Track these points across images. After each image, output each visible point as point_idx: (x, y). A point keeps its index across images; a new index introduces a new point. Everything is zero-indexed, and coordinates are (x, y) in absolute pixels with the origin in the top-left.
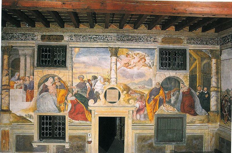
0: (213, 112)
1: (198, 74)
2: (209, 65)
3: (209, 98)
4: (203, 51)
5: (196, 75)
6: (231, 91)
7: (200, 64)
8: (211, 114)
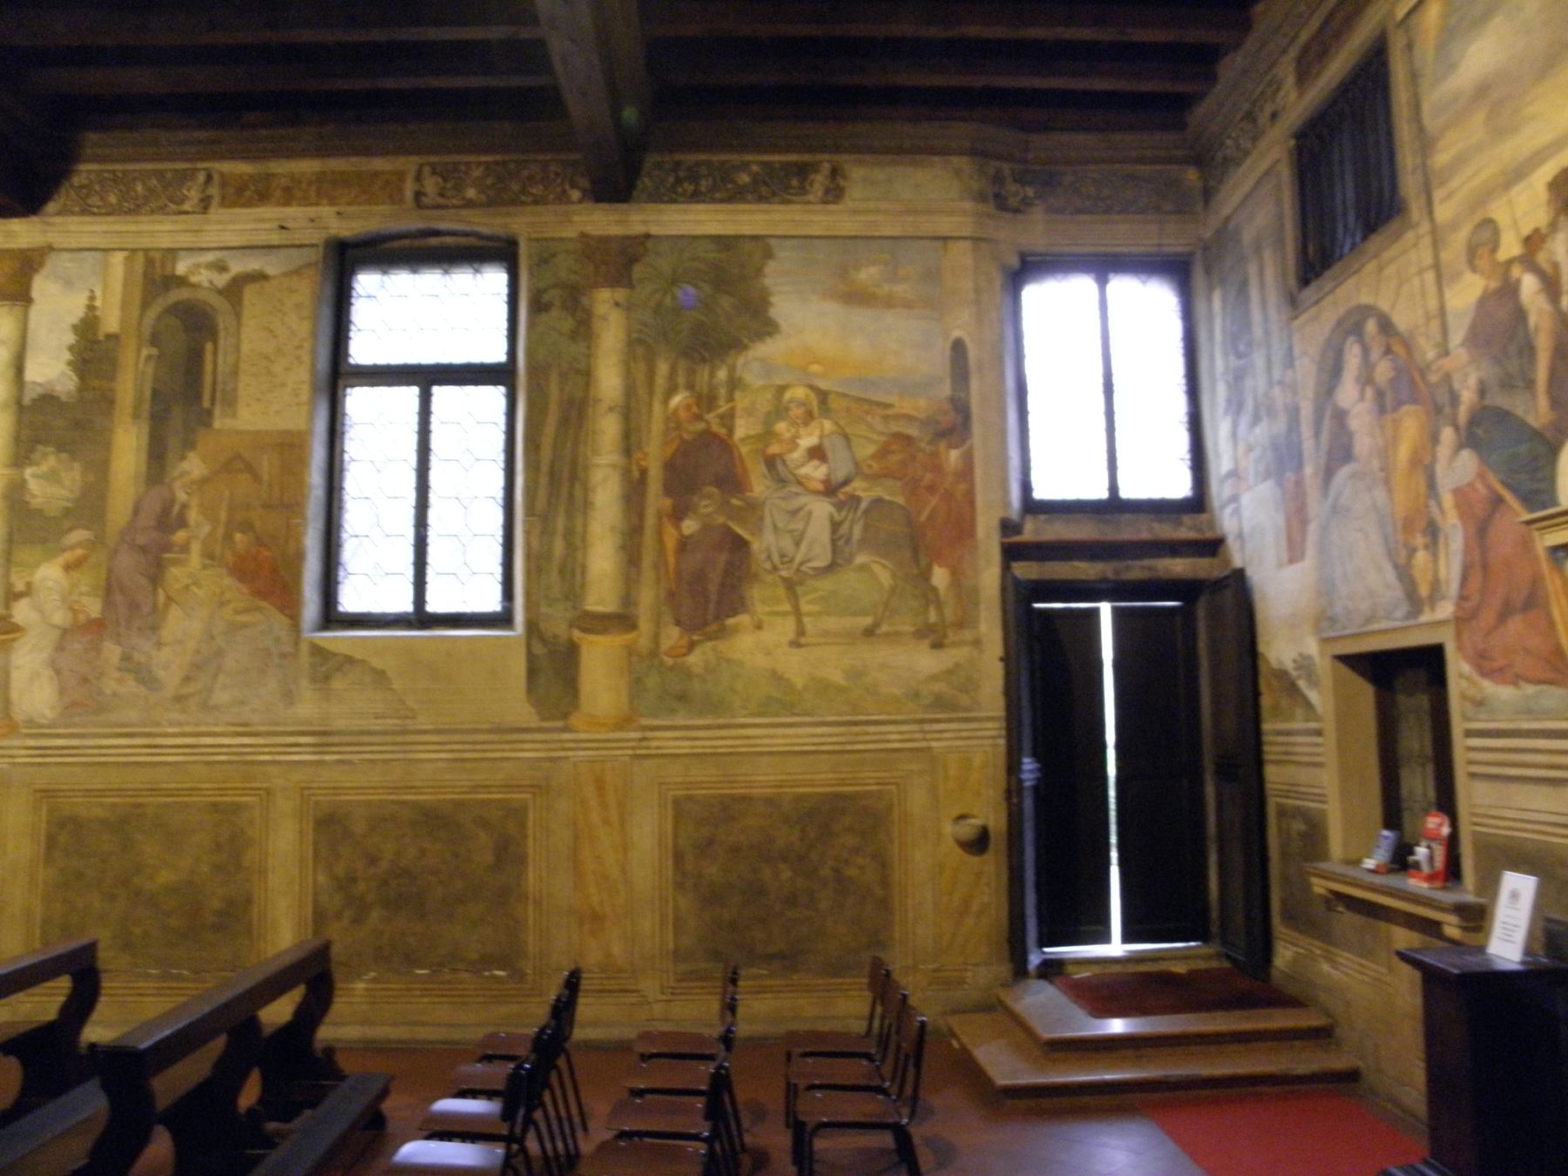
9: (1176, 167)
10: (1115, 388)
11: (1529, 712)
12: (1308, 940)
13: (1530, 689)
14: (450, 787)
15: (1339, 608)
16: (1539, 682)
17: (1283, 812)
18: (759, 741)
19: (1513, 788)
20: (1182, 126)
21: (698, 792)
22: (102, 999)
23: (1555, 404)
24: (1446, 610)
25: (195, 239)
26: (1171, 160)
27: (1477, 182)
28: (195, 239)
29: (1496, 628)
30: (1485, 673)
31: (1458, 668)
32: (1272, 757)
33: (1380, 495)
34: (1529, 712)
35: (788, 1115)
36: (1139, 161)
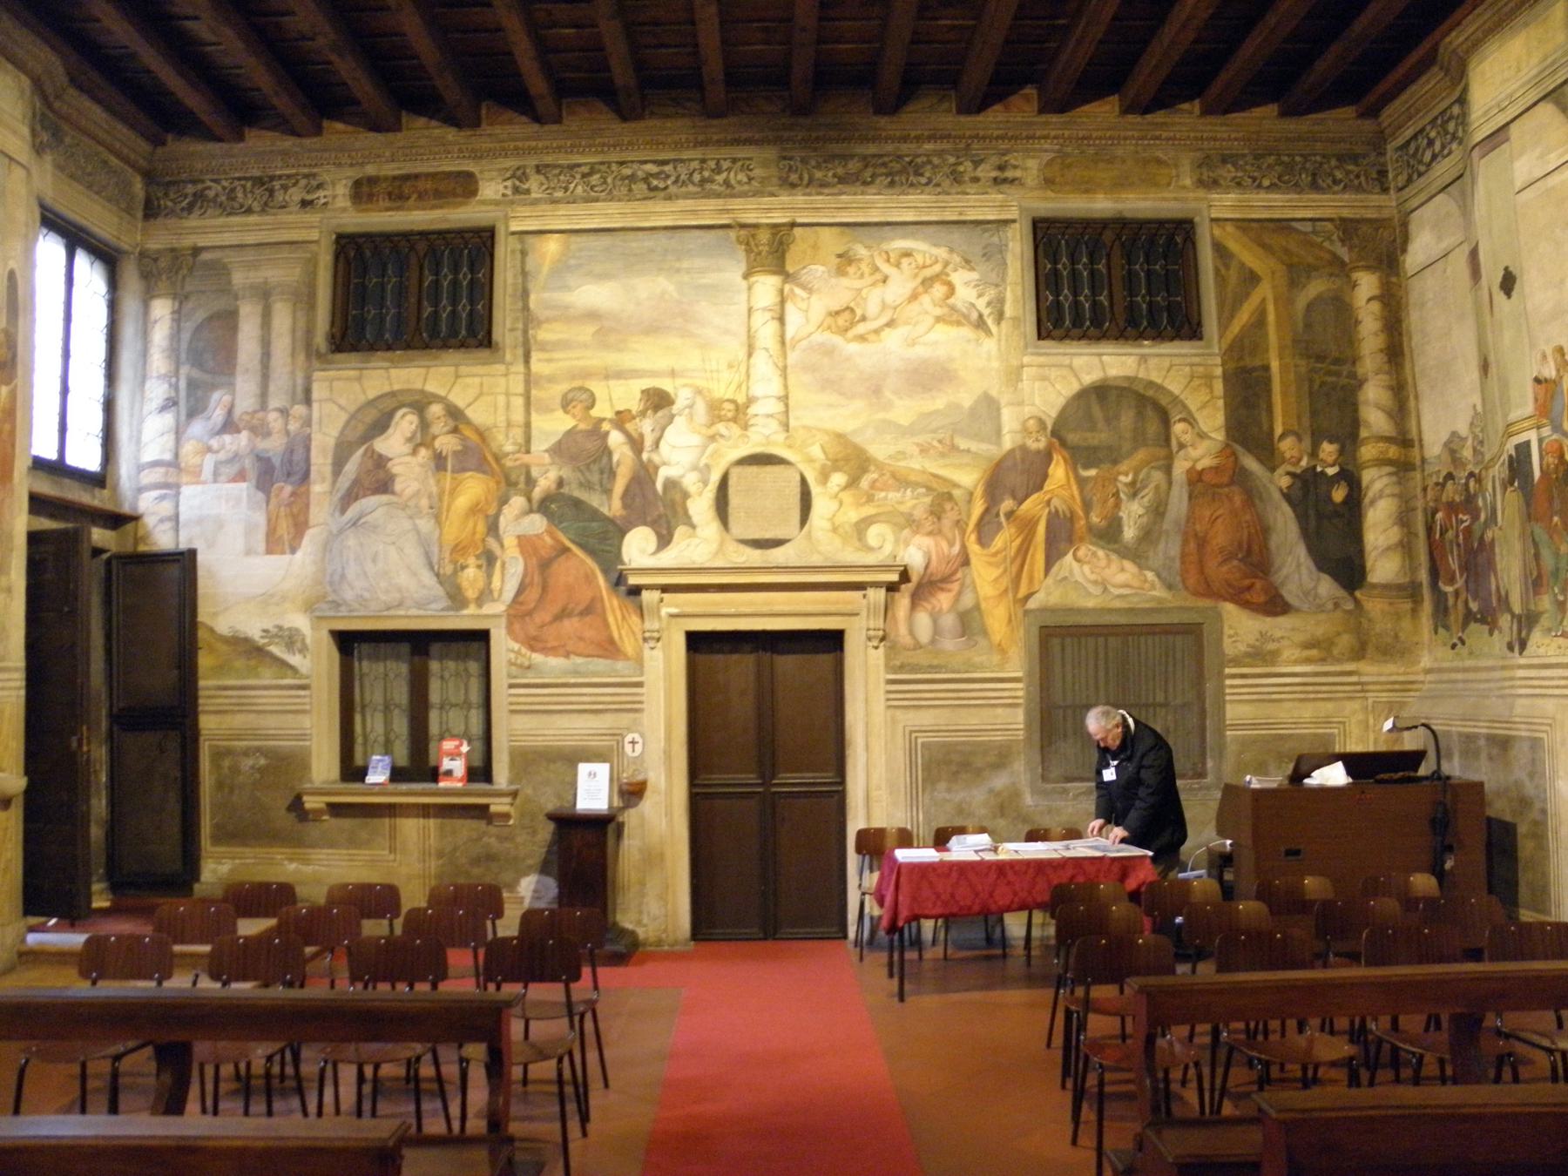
0: (1386, 587)
1: (1275, 365)
2: (1341, 308)
3: (1354, 506)
4: (1294, 224)
5: (1267, 368)
6: (1466, 438)
7: (1285, 302)
8: (1375, 606)
9: (130, 170)
10: (72, 353)
11: (576, 673)
12: (264, 850)
13: (579, 660)
14: (1396, 691)
15: (349, 595)
16: (588, 656)
17: (219, 755)
18: (260, 701)
19: (556, 717)
20: (158, 142)
21: (236, 743)
22: (506, 906)
23: (625, 506)
24: (498, 608)
25: (510, 290)
26: (133, 165)
27: (581, 363)
28: (510, 290)
29: (551, 623)
30: (533, 649)
31: (503, 648)
32: (206, 708)
33: (426, 525)
34: (576, 673)
35: (953, 828)
36: (118, 155)
